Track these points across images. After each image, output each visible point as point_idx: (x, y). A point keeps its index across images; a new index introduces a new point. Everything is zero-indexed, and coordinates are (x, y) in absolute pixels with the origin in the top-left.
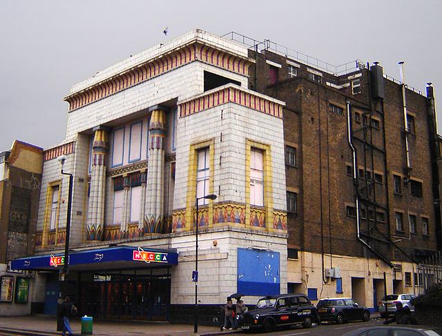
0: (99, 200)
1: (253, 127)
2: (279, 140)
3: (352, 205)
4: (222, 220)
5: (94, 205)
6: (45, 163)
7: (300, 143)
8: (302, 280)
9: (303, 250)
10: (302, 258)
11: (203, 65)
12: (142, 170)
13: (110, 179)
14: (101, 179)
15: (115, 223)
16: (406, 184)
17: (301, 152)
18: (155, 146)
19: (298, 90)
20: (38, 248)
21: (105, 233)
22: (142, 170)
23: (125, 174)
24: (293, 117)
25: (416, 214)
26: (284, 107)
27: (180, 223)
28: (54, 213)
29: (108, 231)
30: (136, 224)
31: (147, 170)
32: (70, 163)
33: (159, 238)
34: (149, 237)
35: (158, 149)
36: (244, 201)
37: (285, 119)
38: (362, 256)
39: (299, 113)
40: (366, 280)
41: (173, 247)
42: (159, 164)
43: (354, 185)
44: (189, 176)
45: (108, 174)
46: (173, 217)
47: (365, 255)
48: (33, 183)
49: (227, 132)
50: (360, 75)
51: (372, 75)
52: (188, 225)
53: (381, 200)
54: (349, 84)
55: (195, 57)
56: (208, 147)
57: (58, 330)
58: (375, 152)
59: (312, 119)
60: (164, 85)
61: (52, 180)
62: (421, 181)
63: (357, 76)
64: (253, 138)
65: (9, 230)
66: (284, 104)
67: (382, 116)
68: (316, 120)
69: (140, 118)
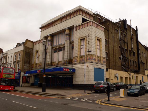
0: (50, 55)
1: (97, 33)
2: (103, 37)
3: (120, 57)
4: (90, 59)
5: (49, 56)
6: (34, 46)
7: (108, 39)
8: (109, 77)
9: (109, 69)
10: (109, 71)
11: (82, 16)
12: (63, 46)
13: (53, 49)
14: (50, 49)
15: (54, 61)
16: (132, 52)
17: (109, 41)
18: (67, 39)
19: (107, 24)
20: (32, 68)
21: (52, 64)
22: (63, 46)
23: (57, 48)
24: (107, 30)
25: (134, 60)
26: (104, 29)
27: (76, 61)
28: (37, 59)
29: (52, 64)
30: (61, 62)
31: (64, 46)
32: (41, 45)
33: (69, 65)
34: (66, 65)
35: (68, 40)
36: (95, 54)
37: (105, 32)
38: (123, 71)
39: (108, 31)
40: (124, 78)
41: (74, 67)
42: (68, 44)
43: (121, 51)
44: (78, 47)
45: (52, 48)
46: (74, 59)
47: (123, 70)
48: (31, 51)
49: (91, 34)
50: (121, 22)
51: (124, 22)
52: (78, 61)
53: (127, 56)
54: (117, 25)
55: (79, 13)
56: (84, 39)
57: (42, 92)
58: (125, 43)
59: (111, 33)
60: (70, 22)
61: (36, 50)
62: (135, 52)
63: (120, 22)
64: (97, 36)
65: (25, 63)
66: (104, 27)
67: (127, 33)
68: (112, 33)
69: (62, 32)
